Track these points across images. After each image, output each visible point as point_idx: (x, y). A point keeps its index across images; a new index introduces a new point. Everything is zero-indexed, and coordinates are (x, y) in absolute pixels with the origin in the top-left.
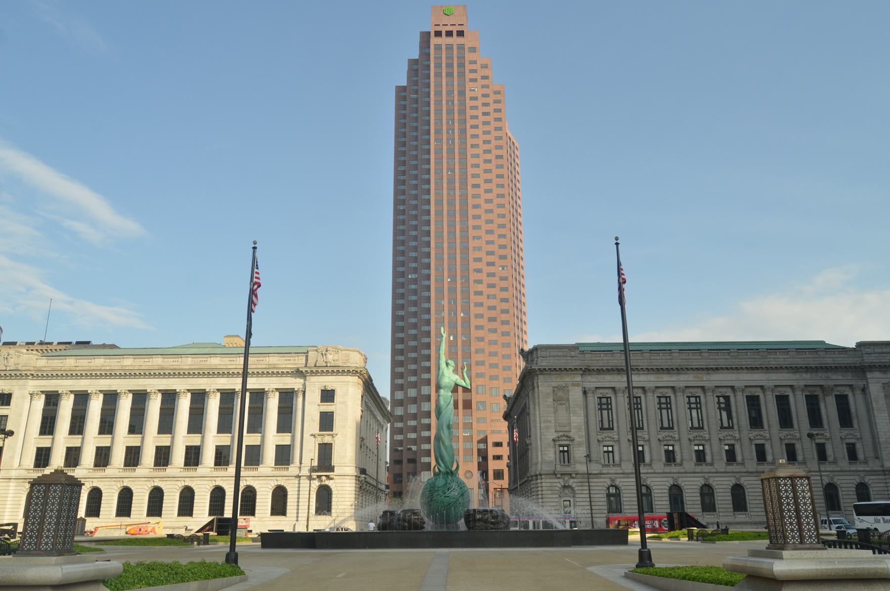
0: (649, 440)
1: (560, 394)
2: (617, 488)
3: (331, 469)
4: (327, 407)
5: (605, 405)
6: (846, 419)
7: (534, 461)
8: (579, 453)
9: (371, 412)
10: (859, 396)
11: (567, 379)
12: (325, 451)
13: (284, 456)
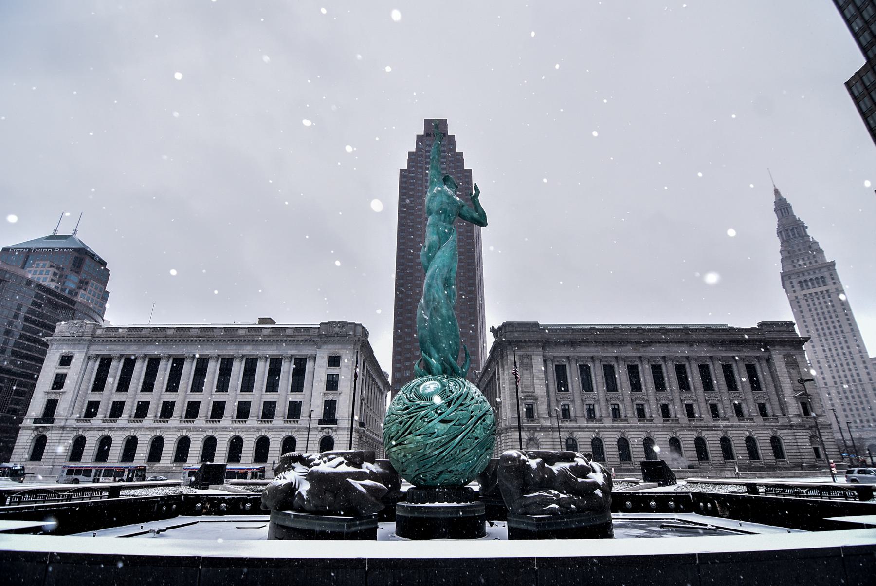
0: (598, 400)
1: (525, 360)
2: (574, 440)
3: (335, 422)
4: (334, 371)
5: (561, 373)
6: (755, 385)
7: (504, 418)
8: (542, 408)
9: (373, 380)
10: (764, 364)
11: (529, 351)
12: (330, 407)
13: (294, 411)
